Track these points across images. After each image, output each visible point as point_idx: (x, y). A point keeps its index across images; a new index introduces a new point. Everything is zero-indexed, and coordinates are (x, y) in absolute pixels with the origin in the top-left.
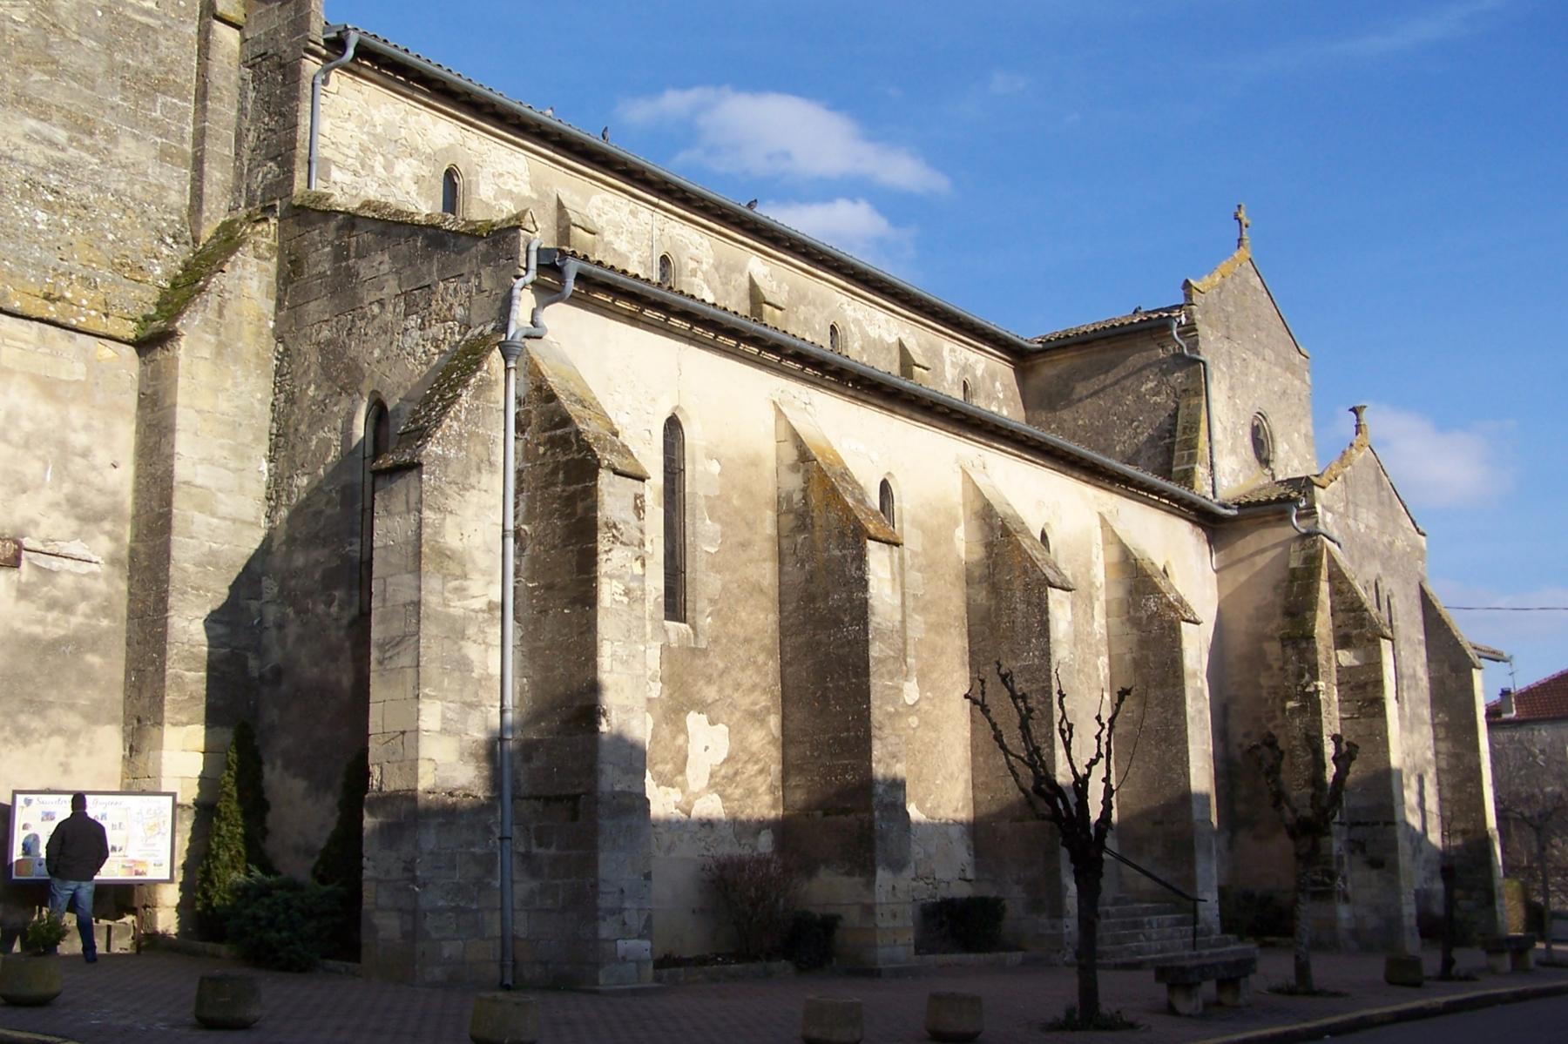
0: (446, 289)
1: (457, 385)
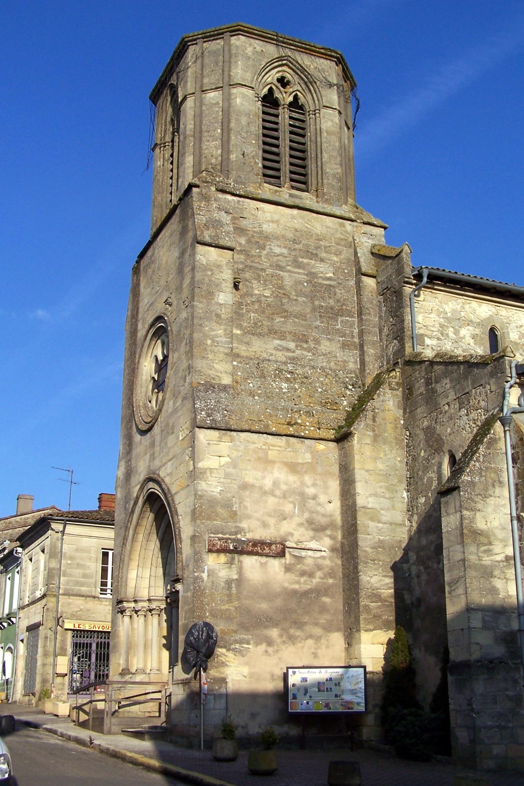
0: (476, 393)
1: (479, 443)
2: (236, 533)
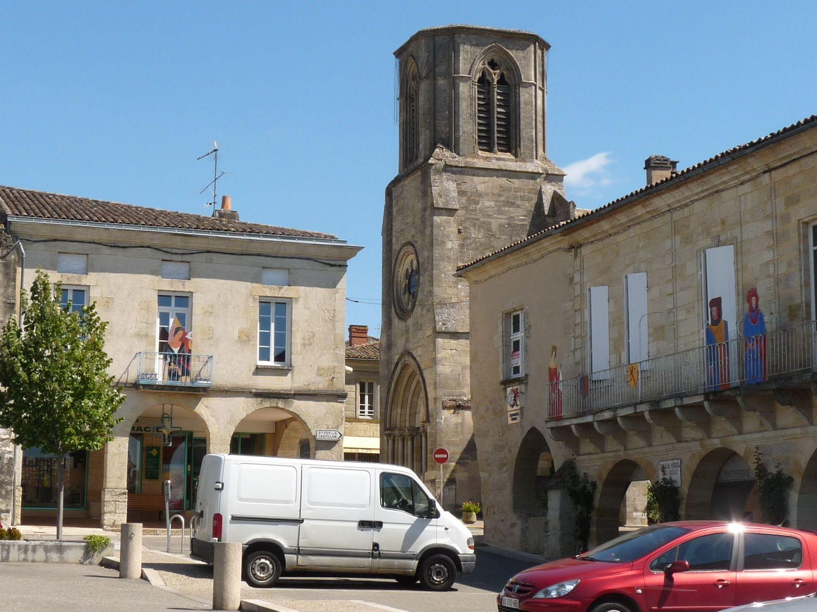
2: (461, 396)
